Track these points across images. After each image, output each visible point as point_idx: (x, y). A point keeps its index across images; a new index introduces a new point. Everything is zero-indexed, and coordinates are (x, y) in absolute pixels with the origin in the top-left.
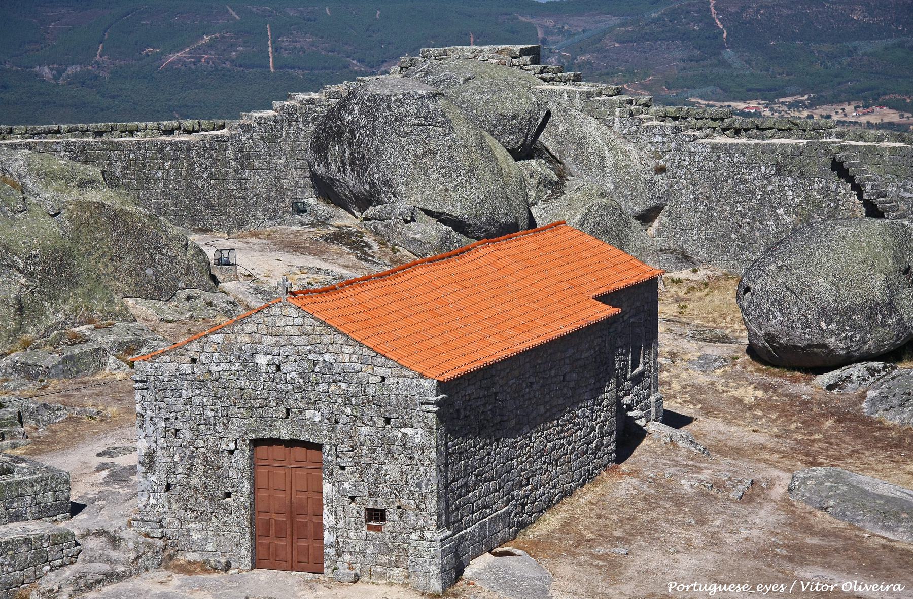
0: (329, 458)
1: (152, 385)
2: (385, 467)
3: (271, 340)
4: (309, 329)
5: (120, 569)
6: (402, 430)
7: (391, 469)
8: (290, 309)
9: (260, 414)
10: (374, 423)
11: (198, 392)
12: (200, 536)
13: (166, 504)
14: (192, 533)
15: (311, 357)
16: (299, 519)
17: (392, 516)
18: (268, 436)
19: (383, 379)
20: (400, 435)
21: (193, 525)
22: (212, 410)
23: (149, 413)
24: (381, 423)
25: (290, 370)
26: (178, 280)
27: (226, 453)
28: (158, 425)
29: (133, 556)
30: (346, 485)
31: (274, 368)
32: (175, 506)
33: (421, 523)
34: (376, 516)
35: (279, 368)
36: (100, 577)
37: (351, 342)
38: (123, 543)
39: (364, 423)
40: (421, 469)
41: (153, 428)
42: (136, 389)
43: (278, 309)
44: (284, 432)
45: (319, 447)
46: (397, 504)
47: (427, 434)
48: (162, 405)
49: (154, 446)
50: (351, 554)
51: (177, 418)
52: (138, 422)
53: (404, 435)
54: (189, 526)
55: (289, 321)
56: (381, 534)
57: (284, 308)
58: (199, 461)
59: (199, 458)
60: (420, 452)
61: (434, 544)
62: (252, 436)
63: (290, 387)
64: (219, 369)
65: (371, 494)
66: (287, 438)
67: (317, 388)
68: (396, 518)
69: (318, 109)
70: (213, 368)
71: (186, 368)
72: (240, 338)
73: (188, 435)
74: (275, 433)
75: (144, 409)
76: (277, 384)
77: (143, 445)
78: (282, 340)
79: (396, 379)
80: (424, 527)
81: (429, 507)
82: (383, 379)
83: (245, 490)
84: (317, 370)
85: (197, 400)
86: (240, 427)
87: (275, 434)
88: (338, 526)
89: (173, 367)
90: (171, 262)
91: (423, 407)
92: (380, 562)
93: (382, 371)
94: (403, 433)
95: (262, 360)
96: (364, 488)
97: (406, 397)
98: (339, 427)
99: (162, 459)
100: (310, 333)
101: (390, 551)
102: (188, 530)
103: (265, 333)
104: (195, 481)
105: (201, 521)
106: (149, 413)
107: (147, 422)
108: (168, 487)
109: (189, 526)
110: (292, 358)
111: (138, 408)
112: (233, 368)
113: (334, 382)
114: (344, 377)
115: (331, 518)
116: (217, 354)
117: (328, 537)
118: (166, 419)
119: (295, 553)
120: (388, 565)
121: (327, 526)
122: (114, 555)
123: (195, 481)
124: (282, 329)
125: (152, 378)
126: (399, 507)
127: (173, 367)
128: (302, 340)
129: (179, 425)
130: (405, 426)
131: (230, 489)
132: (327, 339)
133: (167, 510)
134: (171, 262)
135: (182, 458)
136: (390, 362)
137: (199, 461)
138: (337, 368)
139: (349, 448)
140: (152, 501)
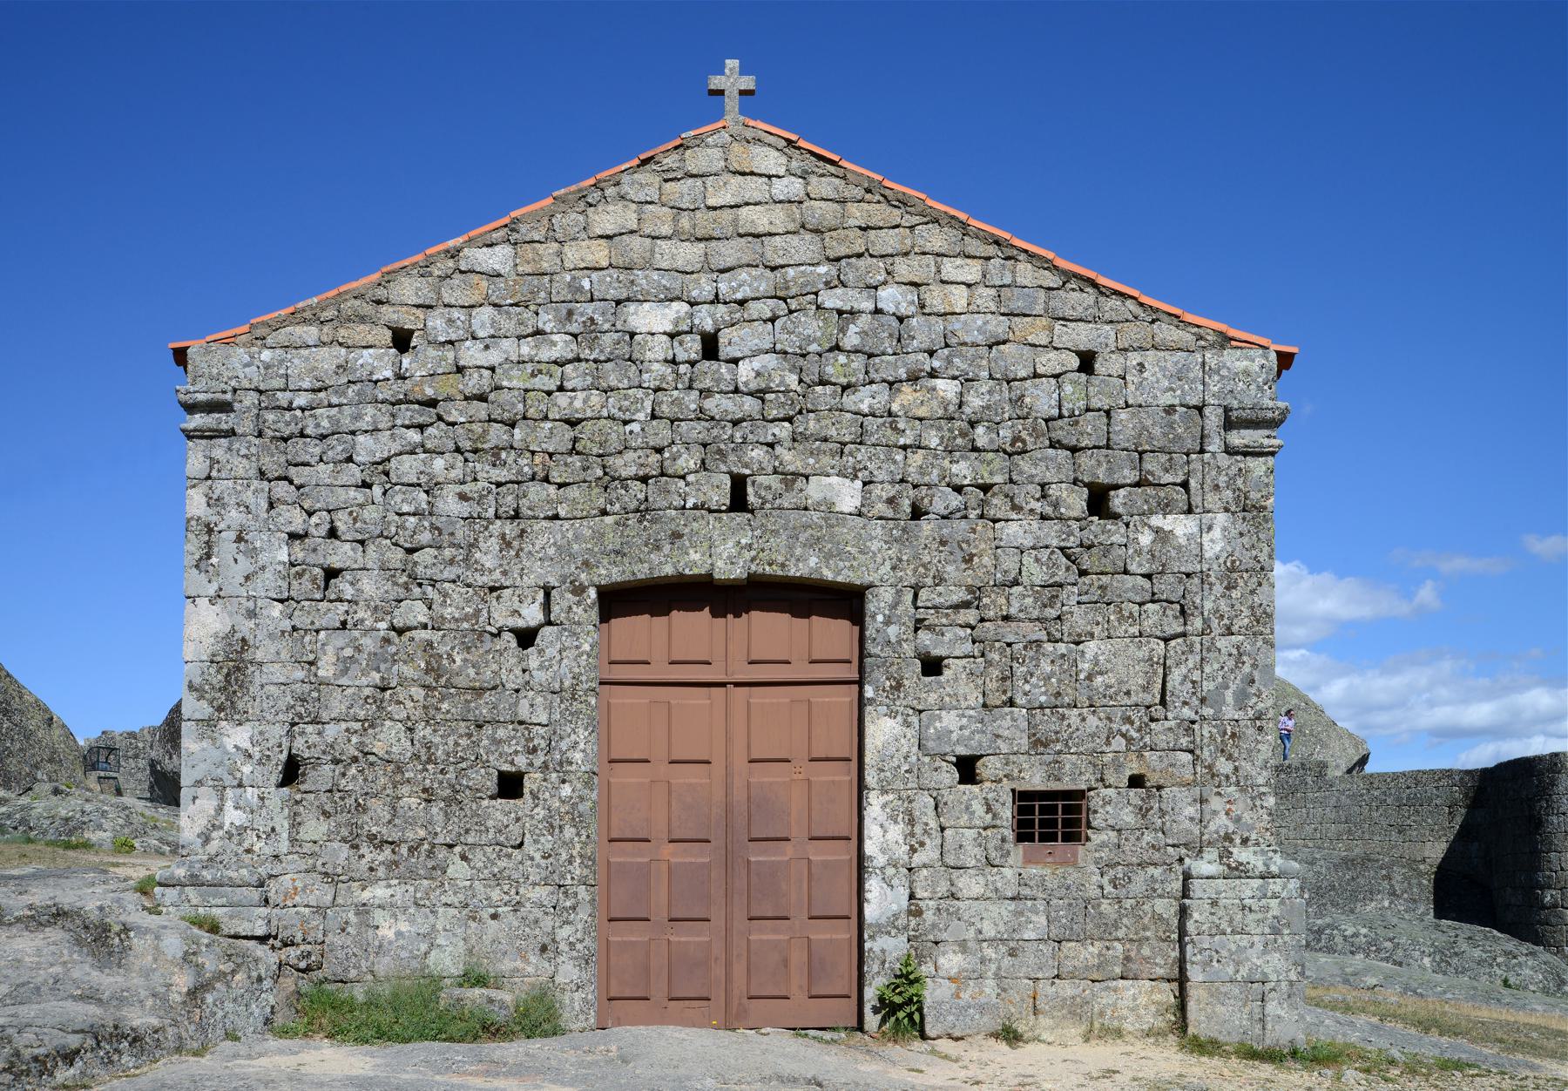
0: (893, 631)
1: (246, 426)
2: (1091, 647)
3: (689, 254)
4: (822, 212)
5: (139, 1018)
6: (1157, 520)
7: (1114, 658)
8: (757, 149)
9: (642, 496)
10: (1056, 506)
11: (414, 436)
12: (404, 927)
13: (283, 825)
14: (379, 917)
15: (831, 300)
16: (759, 856)
17: (1112, 810)
18: (668, 570)
19: (1087, 362)
20: (1146, 539)
21: (379, 892)
22: (463, 497)
23: (234, 516)
24: (1076, 502)
25: (753, 355)
26: (36, 766)
27: (509, 640)
28: (263, 558)
29: (183, 981)
30: (949, 720)
31: (693, 346)
32: (315, 828)
33: (1221, 823)
34: (1049, 818)
35: (710, 347)
36: (73, 1041)
37: (973, 246)
38: (136, 941)
39: (1016, 508)
40: (1222, 643)
41: (245, 566)
42: (189, 435)
43: (716, 153)
44: (725, 553)
45: (846, 602)
46: (1134, 767)
47: (1244, 527)
48: (281, 489)
49: (245, 628)
50: (963, 946)
51: (333, 533)
52: (194, 547)
53: (1161, 535)
54: (366, 895)
55: (753, 188)
56: (1073, 876)
57: (736, 147)
58: (408, 671)
59: (410, 659)
60: (1219, 589)
61: (1275, 886)
62: (612, 573)
63: (750, 405)
64: (494, 357)
65: (1039, 743)
66: (737, 572)
67: (849, 400)
68: (1128, 817)
69: (141, 745)
70: (472, 354)
71: (378, 361)
72: (573, 255)
73: (370, 586)
74: (694, 556)
75: (214, 502)
76: (705, 393)
77: (205, 625)
78: (729, 252)
79: (1134, 358)
80: (1228, 838)
81: (1246, 766)
82: (1087, 362)
83: (578, 756)
84: (851, 339)
85: (407, 468)
86: (572, 545)
87: (694, 562)
88: (918, 859)
89: (327, 359)
90: (27, 738)
91: (1238, 438)
92: (1068, 965)
93: (1083, 336)
94: (1158, 531)
95: (652, 319)
96: (1012, 727)
97: (1170, 409)
98: (926, 527)
99: (274, 670)
100: (830, 221)
101: (1107, 932)
102: (363, 909)
103: (666, 230)
104: (389, 739)
105: (411, 876)
106: (234, 516)
107: (226, 545)
108: (292, 772)
109: (366, 895)
110: (764, 308)
111: (196, 504)
112: (547, 354)
113: (913, 378)
114: (949, 361)
115: (896, 832)
116: (488, 311)
117: (881, 901)
118: (293, 536)
119: (739, 970)
120: (1098, 976)
121: (881, 860)
122: (108, 981)
123: (389, 739)
124: (727, 215)
125: (250, 399)
126: (1136, 781)
127: (327, 359)
128: (803, 247)
129: (341, 554)
130: (1166, 508)
131: (521, 762)
132: (888, 241)
133: (284, 847)
134: (27, 738)
135: (345, 665)
136: (1115, 302)
137: (408, 671)
138: (923, 332)
139: (960, 595)
140: (233, 817)
